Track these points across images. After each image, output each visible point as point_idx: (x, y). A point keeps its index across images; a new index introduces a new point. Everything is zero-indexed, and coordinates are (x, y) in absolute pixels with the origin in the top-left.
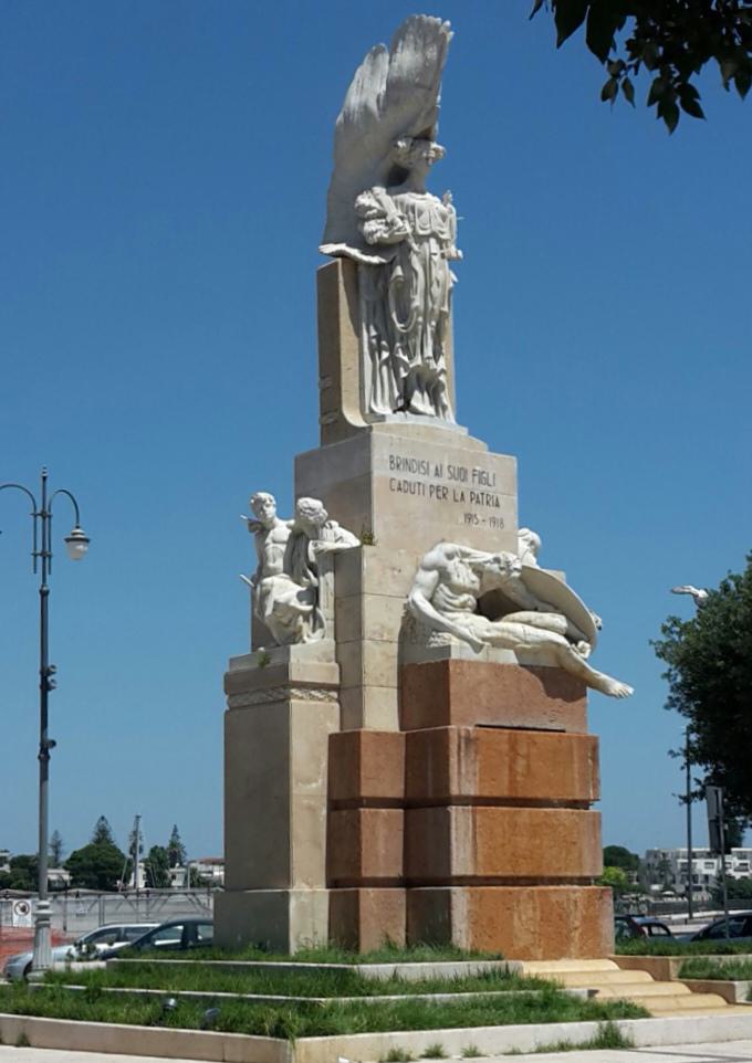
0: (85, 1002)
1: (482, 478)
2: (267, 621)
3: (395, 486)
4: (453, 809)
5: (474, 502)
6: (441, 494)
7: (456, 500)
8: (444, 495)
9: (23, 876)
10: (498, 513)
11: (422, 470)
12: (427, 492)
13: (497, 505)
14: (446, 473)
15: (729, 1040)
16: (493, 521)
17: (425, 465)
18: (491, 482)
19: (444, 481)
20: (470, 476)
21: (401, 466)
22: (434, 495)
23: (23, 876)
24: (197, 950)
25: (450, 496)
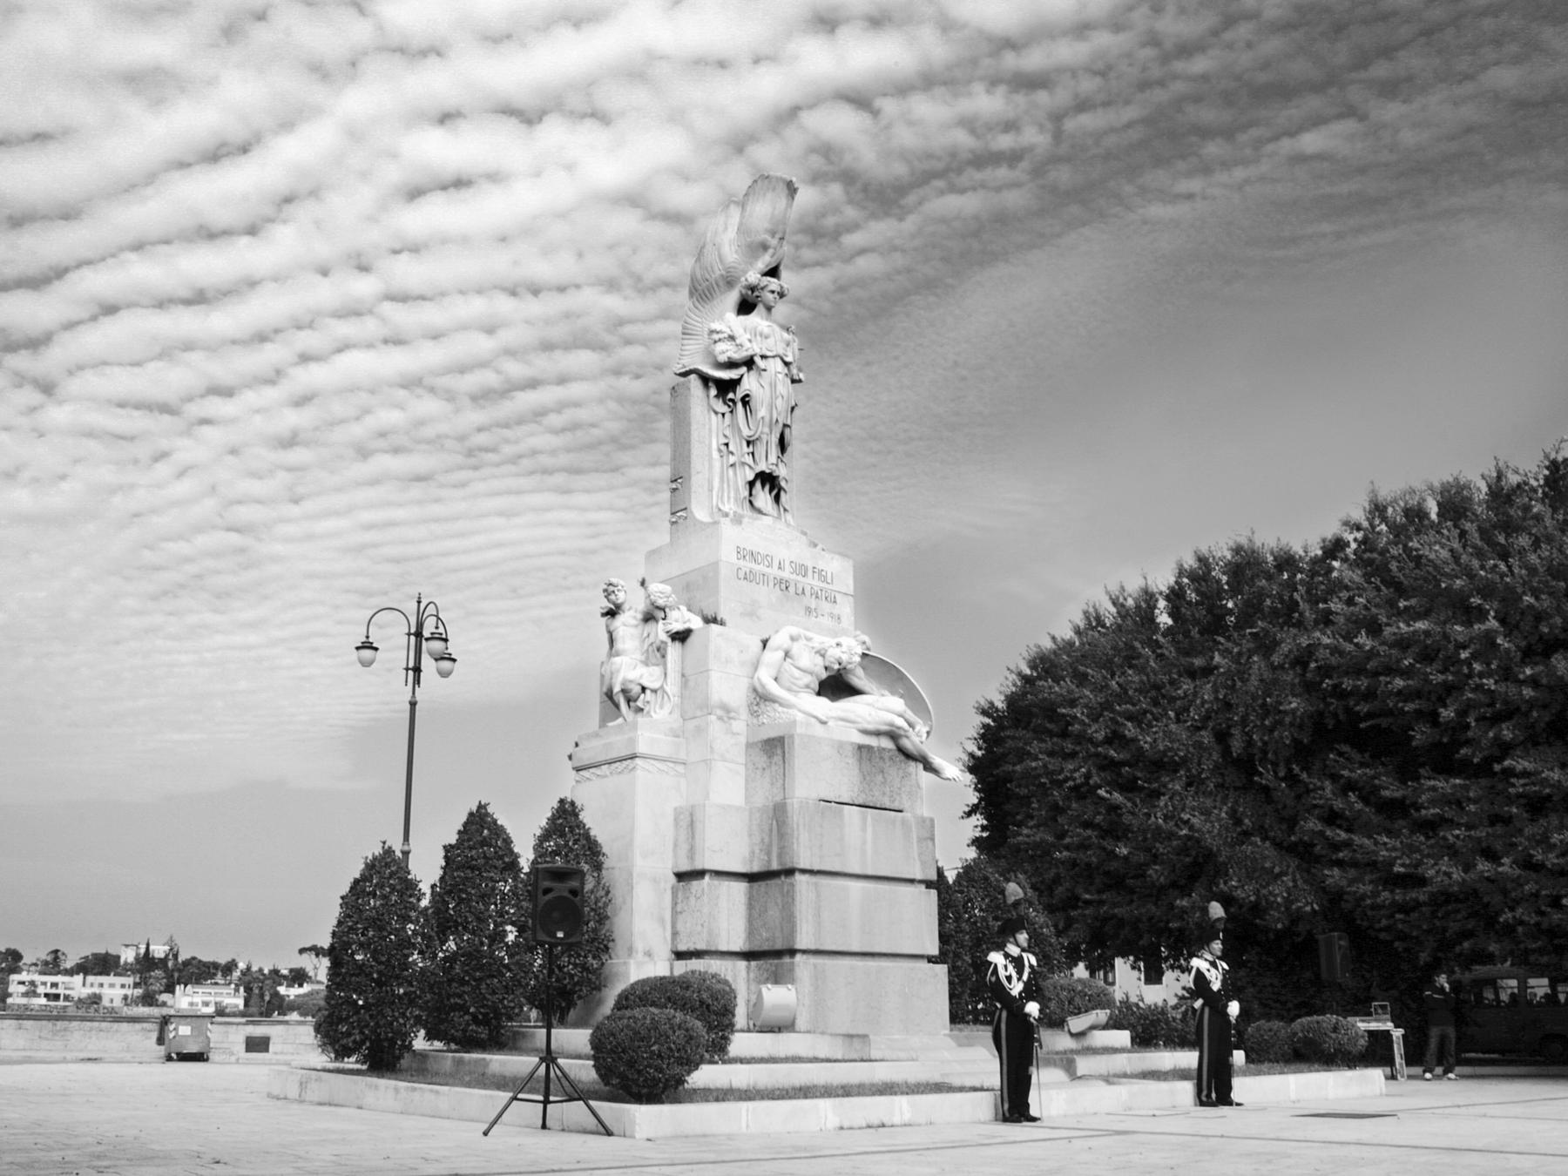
3: (742, 575)
6: (783, 586)
12: (771, 584)
13: (835, 602)
16: (832, 615)
17: (769, 559)
20: (810, 573)
21: (747, 558)
25: (792, 589)
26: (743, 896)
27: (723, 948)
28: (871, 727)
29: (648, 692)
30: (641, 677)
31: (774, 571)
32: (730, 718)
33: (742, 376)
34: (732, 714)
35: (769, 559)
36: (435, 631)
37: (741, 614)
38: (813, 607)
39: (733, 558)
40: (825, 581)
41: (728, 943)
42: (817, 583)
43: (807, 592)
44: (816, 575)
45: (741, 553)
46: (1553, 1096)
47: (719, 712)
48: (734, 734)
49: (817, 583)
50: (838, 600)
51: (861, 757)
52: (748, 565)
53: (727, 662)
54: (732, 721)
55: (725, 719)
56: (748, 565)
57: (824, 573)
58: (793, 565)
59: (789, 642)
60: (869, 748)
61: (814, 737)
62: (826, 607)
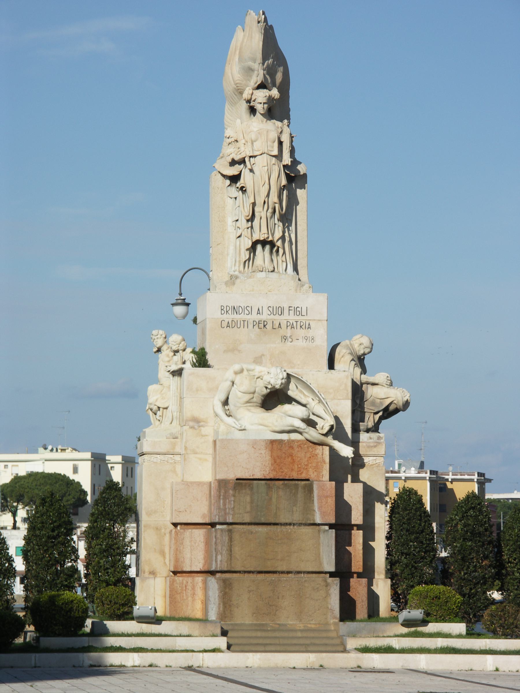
0: (364, 475)
1: (297, 311)
2: (83, 629)
3: (225, 324)
4: (332, 569)
5: (289, 328)
6: (262, 326)
7: (289, 307)
8: (264, 326)
9: (519, 598)
10: (310, 333)
11: (246, 312)
12: (251, 326)
13: (309, 328)
14: (266, 311)
15: (12, 667)
16: (306, 338)
17: (249, 309)
18: (304, 313)
19: (264, 316)
20: (286, 311)
21: (230, 312)
22: (257, 326)
23: (519, 598)
24: (188, 587)
25: (269, 326)
26: (202, 538)
27: (188, 569)
28: (278, 429)
29: (161, 409)
30: (157, 400)
31: (255, 316)
32: (199, 426)
33: (241, 171)
34: (202, 424)
35: (249, 309)
36: (179, 297)
37: (225, 351)
38: (289, 335)
39: (218, 315)
40: (301, 314)
41: (191, 566)
42: (292, 318)
43: (284, 325)
44: (292, 312)
45: (224, 310)
46: (256, 649)
47: (191, 424)
48: (203, 436)
49: (292, 318)
50: (312, 325)
51: (272, 448)
52: (230, 317)
53: (197, 390)
54: (202, 428)
55: (196, 427)
56: (230, 317)
57: (298, 309)
58: (271, 309)
59: (234, 376)
60: (281, 441)
61: (232, 440)
62: (302, 333)
